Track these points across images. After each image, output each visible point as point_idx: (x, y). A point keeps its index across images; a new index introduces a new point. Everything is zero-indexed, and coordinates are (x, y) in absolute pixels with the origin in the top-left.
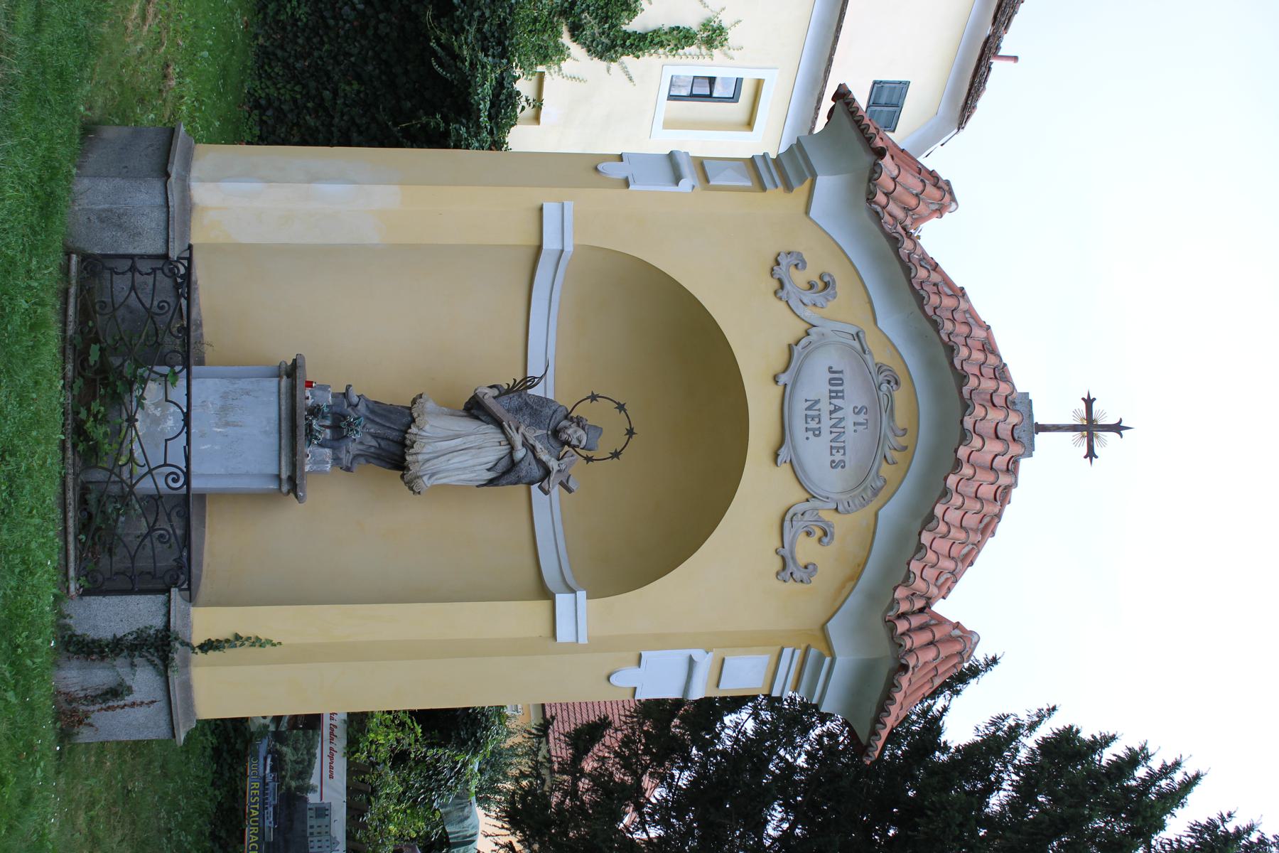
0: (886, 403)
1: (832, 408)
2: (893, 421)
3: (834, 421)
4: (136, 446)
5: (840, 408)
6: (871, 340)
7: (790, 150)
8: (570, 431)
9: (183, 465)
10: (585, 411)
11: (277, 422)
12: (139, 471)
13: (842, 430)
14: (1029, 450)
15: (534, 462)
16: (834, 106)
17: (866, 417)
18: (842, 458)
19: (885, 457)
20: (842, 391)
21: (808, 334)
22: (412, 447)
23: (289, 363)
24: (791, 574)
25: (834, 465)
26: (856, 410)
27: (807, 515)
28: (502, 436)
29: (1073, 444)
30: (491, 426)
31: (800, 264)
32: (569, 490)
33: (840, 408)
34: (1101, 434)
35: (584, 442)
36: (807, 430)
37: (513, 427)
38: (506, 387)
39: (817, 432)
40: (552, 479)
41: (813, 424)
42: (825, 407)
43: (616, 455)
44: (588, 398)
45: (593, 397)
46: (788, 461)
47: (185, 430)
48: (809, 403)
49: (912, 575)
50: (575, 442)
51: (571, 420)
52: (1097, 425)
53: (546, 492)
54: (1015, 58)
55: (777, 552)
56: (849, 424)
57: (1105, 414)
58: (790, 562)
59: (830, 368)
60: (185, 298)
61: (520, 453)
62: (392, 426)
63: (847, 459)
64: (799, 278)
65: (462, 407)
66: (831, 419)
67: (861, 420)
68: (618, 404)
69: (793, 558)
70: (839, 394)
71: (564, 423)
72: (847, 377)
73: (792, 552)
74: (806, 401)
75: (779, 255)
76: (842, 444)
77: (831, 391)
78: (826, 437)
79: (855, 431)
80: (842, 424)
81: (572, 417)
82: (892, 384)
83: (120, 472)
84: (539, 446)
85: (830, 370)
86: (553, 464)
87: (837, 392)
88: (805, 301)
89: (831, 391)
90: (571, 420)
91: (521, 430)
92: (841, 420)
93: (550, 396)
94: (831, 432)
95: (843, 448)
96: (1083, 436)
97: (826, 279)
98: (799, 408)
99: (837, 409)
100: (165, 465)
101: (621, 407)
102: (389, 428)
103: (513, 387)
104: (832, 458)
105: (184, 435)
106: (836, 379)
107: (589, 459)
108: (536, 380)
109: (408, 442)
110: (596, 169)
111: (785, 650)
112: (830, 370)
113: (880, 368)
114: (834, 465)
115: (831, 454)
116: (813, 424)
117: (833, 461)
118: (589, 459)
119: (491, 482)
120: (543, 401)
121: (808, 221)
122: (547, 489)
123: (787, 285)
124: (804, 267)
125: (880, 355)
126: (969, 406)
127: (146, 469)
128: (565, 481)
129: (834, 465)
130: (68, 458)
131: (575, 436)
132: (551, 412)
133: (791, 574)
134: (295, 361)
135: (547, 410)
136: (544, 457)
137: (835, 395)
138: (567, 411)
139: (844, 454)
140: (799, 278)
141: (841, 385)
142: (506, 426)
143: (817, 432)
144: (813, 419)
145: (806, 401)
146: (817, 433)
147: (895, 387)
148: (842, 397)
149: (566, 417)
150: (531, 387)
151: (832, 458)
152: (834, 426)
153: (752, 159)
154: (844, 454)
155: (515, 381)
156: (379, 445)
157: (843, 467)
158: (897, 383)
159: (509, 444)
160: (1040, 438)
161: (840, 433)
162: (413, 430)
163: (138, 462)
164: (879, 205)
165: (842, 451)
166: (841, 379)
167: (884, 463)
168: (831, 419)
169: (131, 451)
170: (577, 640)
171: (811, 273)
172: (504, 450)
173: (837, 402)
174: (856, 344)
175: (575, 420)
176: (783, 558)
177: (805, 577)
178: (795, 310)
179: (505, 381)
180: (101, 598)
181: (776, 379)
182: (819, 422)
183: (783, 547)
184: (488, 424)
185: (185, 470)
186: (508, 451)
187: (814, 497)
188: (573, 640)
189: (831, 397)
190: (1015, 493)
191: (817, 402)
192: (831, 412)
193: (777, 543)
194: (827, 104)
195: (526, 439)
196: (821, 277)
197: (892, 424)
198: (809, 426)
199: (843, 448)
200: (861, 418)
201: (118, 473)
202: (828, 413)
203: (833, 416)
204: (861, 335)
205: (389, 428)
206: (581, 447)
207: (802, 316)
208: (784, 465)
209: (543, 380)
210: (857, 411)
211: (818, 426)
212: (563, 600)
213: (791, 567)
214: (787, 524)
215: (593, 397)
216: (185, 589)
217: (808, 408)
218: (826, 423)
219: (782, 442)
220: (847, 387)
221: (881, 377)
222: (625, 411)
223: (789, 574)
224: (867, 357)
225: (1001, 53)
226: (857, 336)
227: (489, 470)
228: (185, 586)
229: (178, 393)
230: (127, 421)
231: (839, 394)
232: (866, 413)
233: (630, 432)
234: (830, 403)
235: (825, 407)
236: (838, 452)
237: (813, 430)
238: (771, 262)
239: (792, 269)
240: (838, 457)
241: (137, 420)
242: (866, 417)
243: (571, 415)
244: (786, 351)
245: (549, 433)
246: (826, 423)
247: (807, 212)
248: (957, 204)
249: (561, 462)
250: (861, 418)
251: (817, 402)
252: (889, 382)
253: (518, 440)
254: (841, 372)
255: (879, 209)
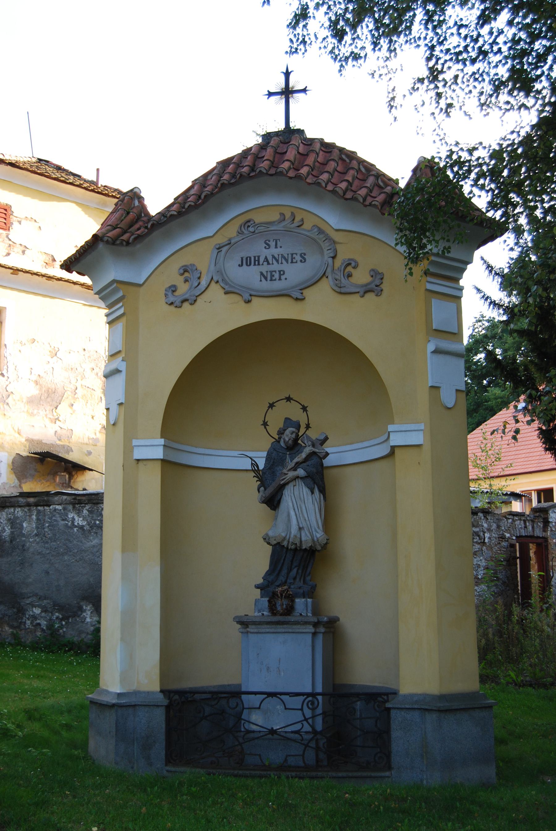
0: (263, 228)
1: (265, 263)
2: (274, 222)
3: (274, 262)
4: (289, 729)
5: (266, 258)
6: (221, 240)
7: (102, 299)
8: (287, 439)
9: (302, 698)
10: (274, 430)
11: (274, 634)
12: (307, 728)
13: (280, 256)
14: (300, 132)
15: (307, 463)
16: (76, 272)
17: (272, 240)
18: (299, 255)
19: (298, 227)
20: (255, 257)
21: (217, 282)
22: (296, 544)
23: (239, 626)
24: (377, 286)
25: (303, 260)
26: (267, 247)
27: (337, 277)
28: (290, 484)
29: (296, 101)
30: (284, 493)
31: (173, 289)
32: (326, 439)
33: (266, 258)
34: (291, 86)
35: (294, 429)
36: (280, 279)
37: (284, 477)
38: (259, 483)
39: (282, 273)
40: (317, 451)
41: (277, 276)
42: (265, 268)
43: (304, 409)
44: (265, 428)
45: (265, 424)
46: (301, 291)
47: (279, 696)
48: (263, 279)
49: (373, 203)
50: (294, 436)
51: (280, 438)
52: (285, 88)
53: (327, 454)
54: (98, 170)
55: (362, 296)
56: (275, 252)
57: (278, 84)
58: (369, 287)
59: (239, 265)
60: (194, 695)
61: (301, 472)
62: (283, 558)
63: (299, 252)
64: (183, 289)
65: (273, 512)
66: (273, 264)
67: (274, 243)
68: (269, 407)
69: (366, 285)
70: (257, 259)
71: (282, 443)
72: (244, 254)
73: (362, 286)
74: (261, 281)
75: (167, 303)
76: (290, 256)
77: (255, 265)
78: (285, 266)
79: (281, 247)
80: (276, 256)
81: (279, 438)
82: (249, 224)
83: (306, 740)
84: (296, 460)
85: (241, 265)
86: (308, 450)
87: (255, 261)
88: (197, 284)
89: (255, 265)
90: (280, 438)
91: (285, 471)
92: (273, 257)
93: (265, 454)
94: (282, 263)
95: (292, 254)
96: (292, 97)
97: (182, 271)
98: (266, 285)
99: (266, 259)
100: (302, 709)
101: (271, 406)
102: (284, 560)
103: (258, 477)
104: (299, 262)
105: (283, 697)
106: (247, 262)
107: (308, 427)
108: (253, 462)
109: (293, 547)
110: (114, 424)
111: (428, 288)
112: (241, 265)
113: (240, 233)
114: (303, 260)
115: (296, 262)
116: (277, 276)
117: (301, 261)
118: (308, 427)
119: (322, 491)
120: (268, 458)
121: (145, 285)
122: (324, 454)
123: (186, 296)
124: (174, 286)
125: (232, 232)
126: (260, 171)
127: (305, 723)
128: (320, 442)
129: (303, 261)
130: (296, 774)
131: (290, 436)
132: (275, 452)
133: (377, 286)
134: (238, 622)
135: (274, 455)
136: (303, 455)
137: (257, 261)
138: (275, 442)
139: (296, 254)
140: (183, 289)
141: (250, 258)
142: (283, 482)
143: (282, 273)
144: (273, 276)
145: (261, 281)
146: (282, 273)
147: (251, 222)
148: (259, 257)
149: (279, 442)
150: (258, 466)
151: (299, 262)
152: (277, 261)
153: (110, 323)
154: (296, 254)
155: (254, 476)
156: (296, 567)
157: (305, 254)
158: (249, 221)
159: (295, 479)
160: (292, 125)
161: (282, 257)
162: (285, 543)
163: (299, 729)
164: (130, 237)
165: (294, 256)
166: (247, 258)
167: (302, 227)
168: (273, 264)
169: (292, 732)
170: (422, 430)
171: (179, 281)
172: (299, 482)
173: (262, 260)
174: (224, 249)
175: (280, 436)
176: (366, 292)
177: (379, 277)
178: (202, 291)
179: (255, 483)
180: (392, 755)
181: (249, 302)
182: (275, 271)
183: (359, 292)
184: (283, 494)
185: (305, 696)
186: (300, 480)
187: (325, 273)
188: (422, 432)
189: (259, 264)
190: (327, 140)
191: (262, 274)
192: (268, 264)
193: (357, 296)
194: (74, 276)
195: (291, 468)
196: (182, 274)
197: (276, 223)
198: (278, 278)
199: (292, 254)
200: (272, 244)
201: (307, 742)
202: (269, 266)
203: (271, 262)
204: (217, 247)
205: (284, 560)
206: (297, 431)
207: (206, 286)
208: (304, 294)
209: (254, 459)
210: (268, 246)
211: (278, 272)
212: (395, 440)
213: (373, 286)
214: (343, 290)
215: (265, 424)
216: (388, 697)
217: (266, 279)
218: (275, 267)
219: (289, 296)
220: (252, 254)
221: (245, 232)
222: (274, 403)
223: (376, 288)
224: (233, 241)
225: (95, 180)
226: (219, 248)
227: (312, 493)
228: (385, 697)
229: (255, 700)
230: (272, 735)
231: (257, 259)
232: (269, 241)
233: (289, 399)
234: (263, 264)
235: (265, 268)
236: (294, 258)
237: (280, 275)
238: (172, 308)
239: (176, 294)
240: (298, 258)
241: (272, 728)
242: (272, 240)
243: (277, 438)
244: (228, 296)
245: (288, 453)
246: (275, 267)
247: (140, 286)
248: (135, 188)
249: (307, 445)
250: (272, 244)
251: (262, 274)
252: (249, 226)
253: (291, 474)
254: (242, 258)
255: (133, 237)
